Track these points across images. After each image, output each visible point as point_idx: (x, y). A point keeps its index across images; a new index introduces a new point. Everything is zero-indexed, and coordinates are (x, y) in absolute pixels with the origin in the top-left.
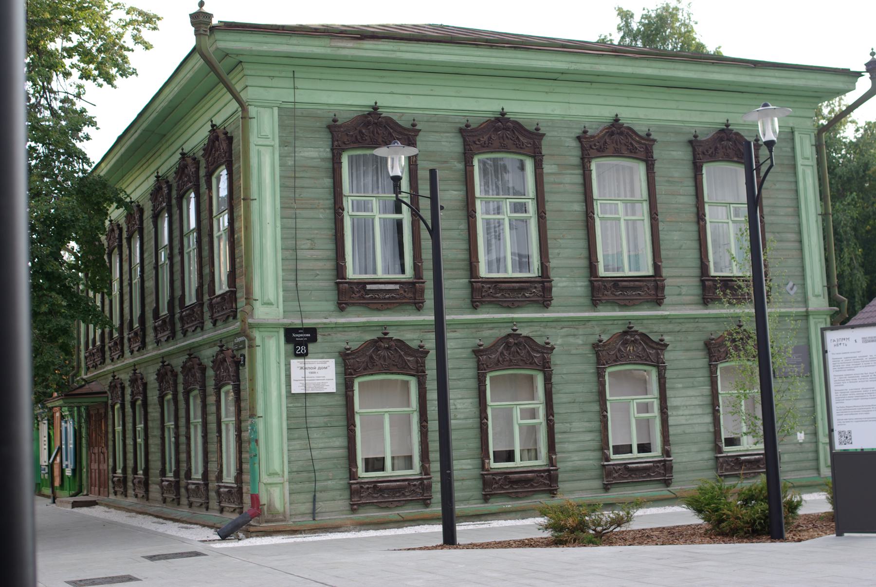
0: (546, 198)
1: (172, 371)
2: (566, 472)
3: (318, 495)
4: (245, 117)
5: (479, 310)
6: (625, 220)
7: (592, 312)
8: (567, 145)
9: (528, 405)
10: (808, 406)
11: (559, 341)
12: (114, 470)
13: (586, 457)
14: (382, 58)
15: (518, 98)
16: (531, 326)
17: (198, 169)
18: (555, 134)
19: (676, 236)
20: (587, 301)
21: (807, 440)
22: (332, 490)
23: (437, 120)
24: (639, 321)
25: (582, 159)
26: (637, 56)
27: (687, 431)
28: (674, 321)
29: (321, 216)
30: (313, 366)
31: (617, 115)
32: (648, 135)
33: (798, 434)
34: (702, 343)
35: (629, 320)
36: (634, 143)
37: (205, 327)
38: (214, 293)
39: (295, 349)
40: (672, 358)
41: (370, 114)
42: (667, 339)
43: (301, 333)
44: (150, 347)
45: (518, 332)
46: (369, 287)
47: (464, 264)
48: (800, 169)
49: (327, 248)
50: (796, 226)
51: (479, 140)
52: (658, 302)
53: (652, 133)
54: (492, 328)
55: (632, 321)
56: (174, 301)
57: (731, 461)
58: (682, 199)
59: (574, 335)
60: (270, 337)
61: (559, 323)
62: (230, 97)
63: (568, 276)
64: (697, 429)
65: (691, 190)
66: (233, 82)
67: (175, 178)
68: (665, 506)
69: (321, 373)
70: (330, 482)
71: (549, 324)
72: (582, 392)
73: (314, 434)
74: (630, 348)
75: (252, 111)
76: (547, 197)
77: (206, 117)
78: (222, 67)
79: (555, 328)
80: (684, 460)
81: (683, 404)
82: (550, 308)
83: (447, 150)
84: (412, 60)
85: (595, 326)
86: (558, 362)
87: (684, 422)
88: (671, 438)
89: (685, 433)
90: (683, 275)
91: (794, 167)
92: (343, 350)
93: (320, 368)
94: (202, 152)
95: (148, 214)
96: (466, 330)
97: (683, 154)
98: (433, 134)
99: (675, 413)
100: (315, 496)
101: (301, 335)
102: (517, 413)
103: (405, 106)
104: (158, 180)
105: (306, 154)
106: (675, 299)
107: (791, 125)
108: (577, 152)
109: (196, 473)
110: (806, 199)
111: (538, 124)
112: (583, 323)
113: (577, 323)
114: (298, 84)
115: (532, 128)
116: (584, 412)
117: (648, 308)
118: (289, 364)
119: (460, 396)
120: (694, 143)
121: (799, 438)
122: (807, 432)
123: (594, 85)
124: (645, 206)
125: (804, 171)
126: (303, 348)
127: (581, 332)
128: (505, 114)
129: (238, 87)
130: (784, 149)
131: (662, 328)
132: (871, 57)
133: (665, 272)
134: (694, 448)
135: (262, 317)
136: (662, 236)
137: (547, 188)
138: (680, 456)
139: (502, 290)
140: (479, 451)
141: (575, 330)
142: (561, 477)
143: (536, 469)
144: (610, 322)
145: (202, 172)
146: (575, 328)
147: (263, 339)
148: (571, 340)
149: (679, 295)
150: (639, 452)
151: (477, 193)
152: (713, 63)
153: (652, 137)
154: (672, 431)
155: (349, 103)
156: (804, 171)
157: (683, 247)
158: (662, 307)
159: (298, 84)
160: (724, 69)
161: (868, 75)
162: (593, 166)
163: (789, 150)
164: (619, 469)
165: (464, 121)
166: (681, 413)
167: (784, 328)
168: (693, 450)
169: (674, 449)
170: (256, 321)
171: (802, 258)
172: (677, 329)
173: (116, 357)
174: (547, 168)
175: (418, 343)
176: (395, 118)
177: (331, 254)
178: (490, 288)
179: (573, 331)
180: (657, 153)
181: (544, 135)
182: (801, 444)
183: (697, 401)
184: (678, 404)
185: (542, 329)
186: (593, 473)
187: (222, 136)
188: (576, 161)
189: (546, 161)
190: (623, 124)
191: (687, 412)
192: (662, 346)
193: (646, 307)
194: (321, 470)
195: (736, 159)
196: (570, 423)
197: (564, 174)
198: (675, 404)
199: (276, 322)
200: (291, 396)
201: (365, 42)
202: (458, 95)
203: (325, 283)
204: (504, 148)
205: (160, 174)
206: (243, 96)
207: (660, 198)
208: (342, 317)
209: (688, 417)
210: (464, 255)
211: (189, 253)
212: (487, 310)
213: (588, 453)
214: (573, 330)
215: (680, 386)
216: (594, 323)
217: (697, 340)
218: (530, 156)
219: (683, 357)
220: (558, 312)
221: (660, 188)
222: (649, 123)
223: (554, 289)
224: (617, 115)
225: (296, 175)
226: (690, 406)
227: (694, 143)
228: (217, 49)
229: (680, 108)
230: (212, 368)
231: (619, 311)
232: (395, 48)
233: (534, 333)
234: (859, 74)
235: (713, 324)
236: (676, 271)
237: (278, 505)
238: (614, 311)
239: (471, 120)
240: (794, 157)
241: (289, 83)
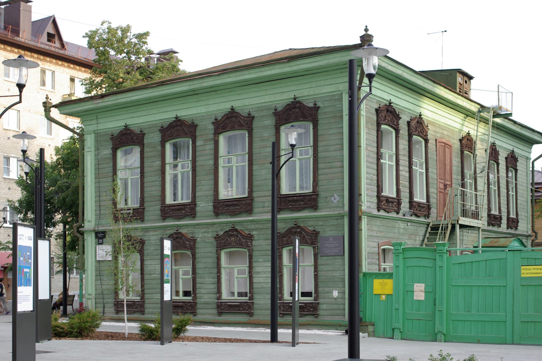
2: (201, 304)
3: (105, 305)
5: (166, 220)
6: (236, 166)
7: (216, 219)
8: (209, 128)
10: (342, 275)
11: (200, 236)
13: (211, 297)
14: (114, 104)
15: (184, 108)
16: (188, 228)
18: (203, 123)
20: (160, 218)
21: (340, 296)
22: (110, 303)
24: (241, 224)
27: (264, 287)
28: (259, 223)
29: (109, 180)
31: (232, 106)
32: (249, 114)
33: (334, 292)
35: (233, 223)
36: (241, 121)
39: (99, 241)
40: (258, 244)
42: (254, 233)
43: (101, 234)
53: (317, 103)
54: (171, 229)
55: (234, 224)
57: (287, 306)
59: (208, 232)
60: (89, 236)
61: (200, 226)
63: (205, 200)
68: (236, 327)
70: (109, 300)
71: (196, 226)
72: (210, 263)
73: (105, 278)
74: (233, 239)
79: (198, 228)
80: (262, 303)
81: (262, 271)
82: (196, 218)
84: (125, 102)
85: (218, 227)
86: (200, 246)
87: (262, 281)
88: (254, 290)
89: (263, 288)
90: (266, 195)
96: (160, 231)
97: (270, 122)
98: (151, 134)
99: (257, 276)
100: (104, 305)
101: (101, 235)
102: (181, 272)
103: (138, 123)
105: (104, 153)
106: (261, 209)
111: (192, 120)
112: (211, 225)
113: (209, 226)
116: (211, 273)
117: (246, 216)
118: (96, 248)
119: (157, 263)
121: (334, 295)
122: (340, 291)
123: (218, 92)
126: (101, 240)
127: (210, 230)
128: (234, 109)
130: (337, 106)
131: (253, 227)
132: (46, 100)
133: (255, 194)
135: (87, 227)
136: (254, 173)
139: (290, 201)
141: (208, 229)
142: (198, 306)
143: (185, 301)
144: (225, 225)
146: (208, 228)
148: (206, 235)
150: (238, 296)
152: (263, 65)
154: (255, 286)
155: (117, 126)
157: (267, 178)
158: (253, 215)
159: (100, 121)
160: (271, 67)
164: (224, 305)
166: (261, 276)
167: (329, 224)
168: (267, 298)
169: (255, 296)
170: (86, 229)
172: (261, 227)
174: (199, 143)
178: (168, 209)
181: (197, 125)
182: (335, 299)
184: (260, 271)
185: (193, 229)
191: (264, 276)
192: (250, 237)
193: (244, 215)
194: (106, 294)
195: (301, 119)
197: (206, 145)
198: (258, 270)
201: (105, 98)
202: (159, 112)
203: (108, 211)
204: (178, 136)
207: (255, 151)
208: (164, 222)
209: (265, 278)
210: (160, 194)
212: (169, 220)
213: (212, 295)
214: (207, 229)
215: (261, 260)
216: (217, 225)
219: (264, 244)
220: (200, 220)
222: (252, 107)
225: (99, 163)
226: (266, 272)
229: (267, 94)
231: (230, 218)
232: (117, 98)
233: (189, 232)
235: (283, 223)
236: (262, 194)
237: (90, 307)
238: (228, 218)
239: (278, 106)
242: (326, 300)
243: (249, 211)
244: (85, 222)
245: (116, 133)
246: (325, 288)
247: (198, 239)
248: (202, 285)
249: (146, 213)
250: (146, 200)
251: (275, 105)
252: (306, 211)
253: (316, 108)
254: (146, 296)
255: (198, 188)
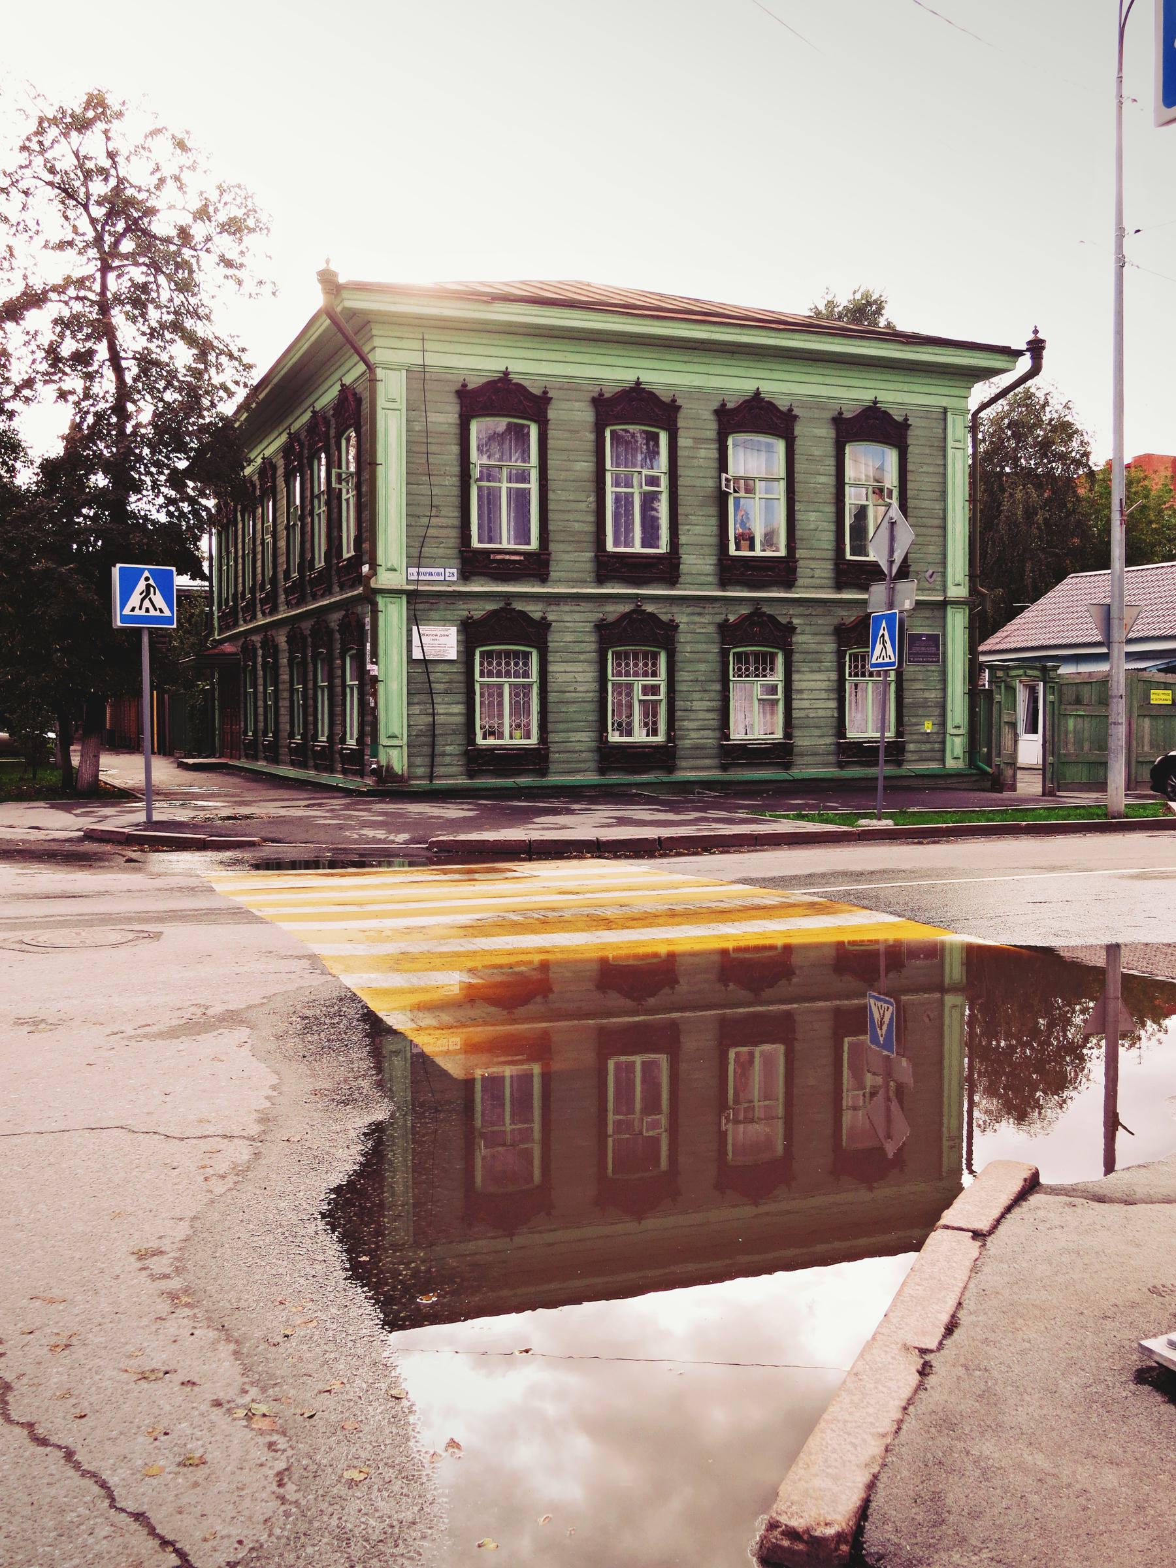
0: (679, 473)
1: (302, 633)
4: (373, 381)
9: (650, 681)
12: (246, 734)
17: (328, 428)
19: (813, 516)
21: (934, 731)
23: (571, 386)
25: (719, 433)
26: (782, 327)
27: (811, 715)
30: (434, 633)
31: (758, 389)
34: (832, 628)
37: (333, 591)
38: (341, 556)
41: (500, 380)
42: (796, 621)
44: (281, 609)
45: (643, 608)
46: (492, 557)
47: (591, 538)
48: (950, 452)
49: (451, 515)
50: (941, 512)
51: (612, 411)
52: (789, 584)
56: (306, 564)
58: (822, 479)
62: (358, 358)
64: (821, 713)
65: (832, 470)
66: (360, 343)
67: (306, 437)
69: (443, 640)
70: (448, 747)
75: (380, 373)
76: (680, 472)
77: (336, 376)
78: (349, 329)
83: (577, 419)
91: (944, 449)
92: (463, 618)
93: (441, 636)
94: (331, 412)
95: (280, 471)
97: (827, 432)
104: (289, 438)
106: (807, 581)
107: (944, 405)
108: (714, 425)
109: (323, 735)
110: (954, 483)
114: (428, 346)
115: (666, 399)
120: (839, 421)
122: (936, 722)
124: (782, 486)
125: (954, 454)
128: (641, 383)
129: (366, 349)
134: (816, 732)
137: (680, 462)
138: (803, 741)
140: (598, 724)
145: (332, 432)
147: (386, 606)
148: (697, 619)
149: (812, 577)
151: (608, 466)
153: (793, 413)
154: (795, 714)
156: (954, 454)
158: (550, 583)
161: (1028, 354)
162: (730, 441)
163: (941, 431)
165: (598, 389)
171: (945, 546)
173: (248, 618)
174: (682, 442)
175: (541, 614)
176: (526, 384)
177: (457, 522)
179: (698, 610)
180: (798, 430)
183: (825, 685)
186: (715, 751)
187: (350, 398)
188: (712, 434)
189: (681, 433)
190: (764, 398)
192: (791, 629)
196: (691, 701)
199: (399, 588)
200: (411, 661)
205: (292, 431)
206: (372, 358)
207: (798, 477)
210: (591, 528)
211: (319, 515)
217: (827, 622)
218: (535, 421)
221: (799, 467)
223: (681, 566)
224: (758, 389)
227: (839, 421)
228: (344, 308)
230: (338, 631)
234: (1019, 353)
238: (533, 587)
240: (945, 439)
241: (418, 345)
242: (915, 737)
243: (789, 583)
244: (380, 570)
245: (474, 382)
246: (911, 718)
247: (682, 626)
248: (686, 714)
249: (553, 566)
250: (552, 536)
251: (840, 405)
252: (609, 585)
253: (905, 426)
254: (552, 737)
255: (682, 529)
